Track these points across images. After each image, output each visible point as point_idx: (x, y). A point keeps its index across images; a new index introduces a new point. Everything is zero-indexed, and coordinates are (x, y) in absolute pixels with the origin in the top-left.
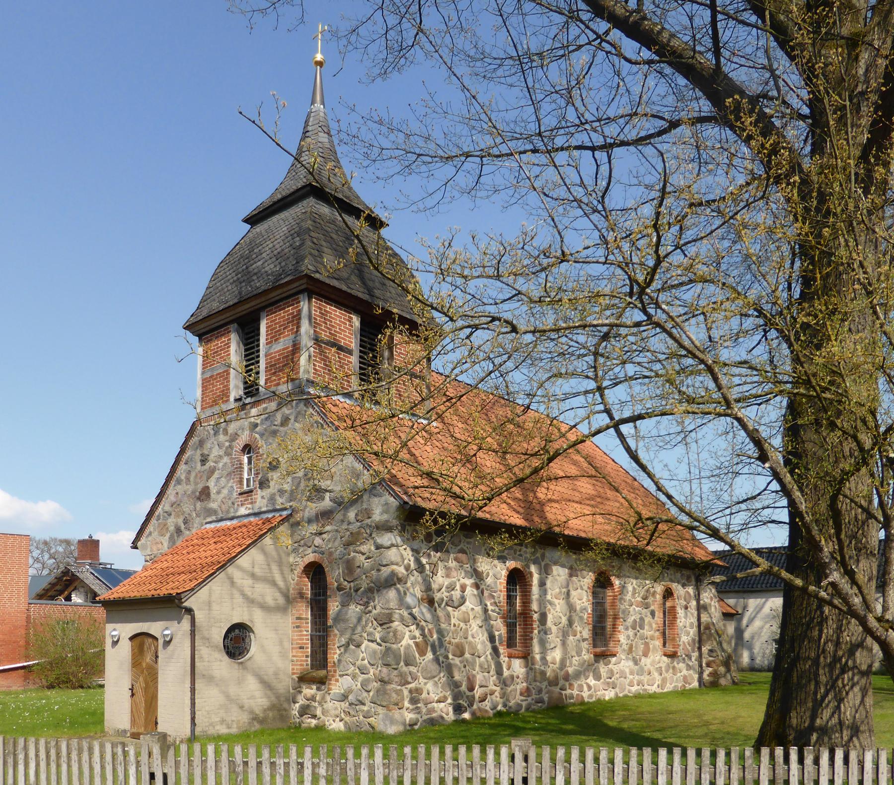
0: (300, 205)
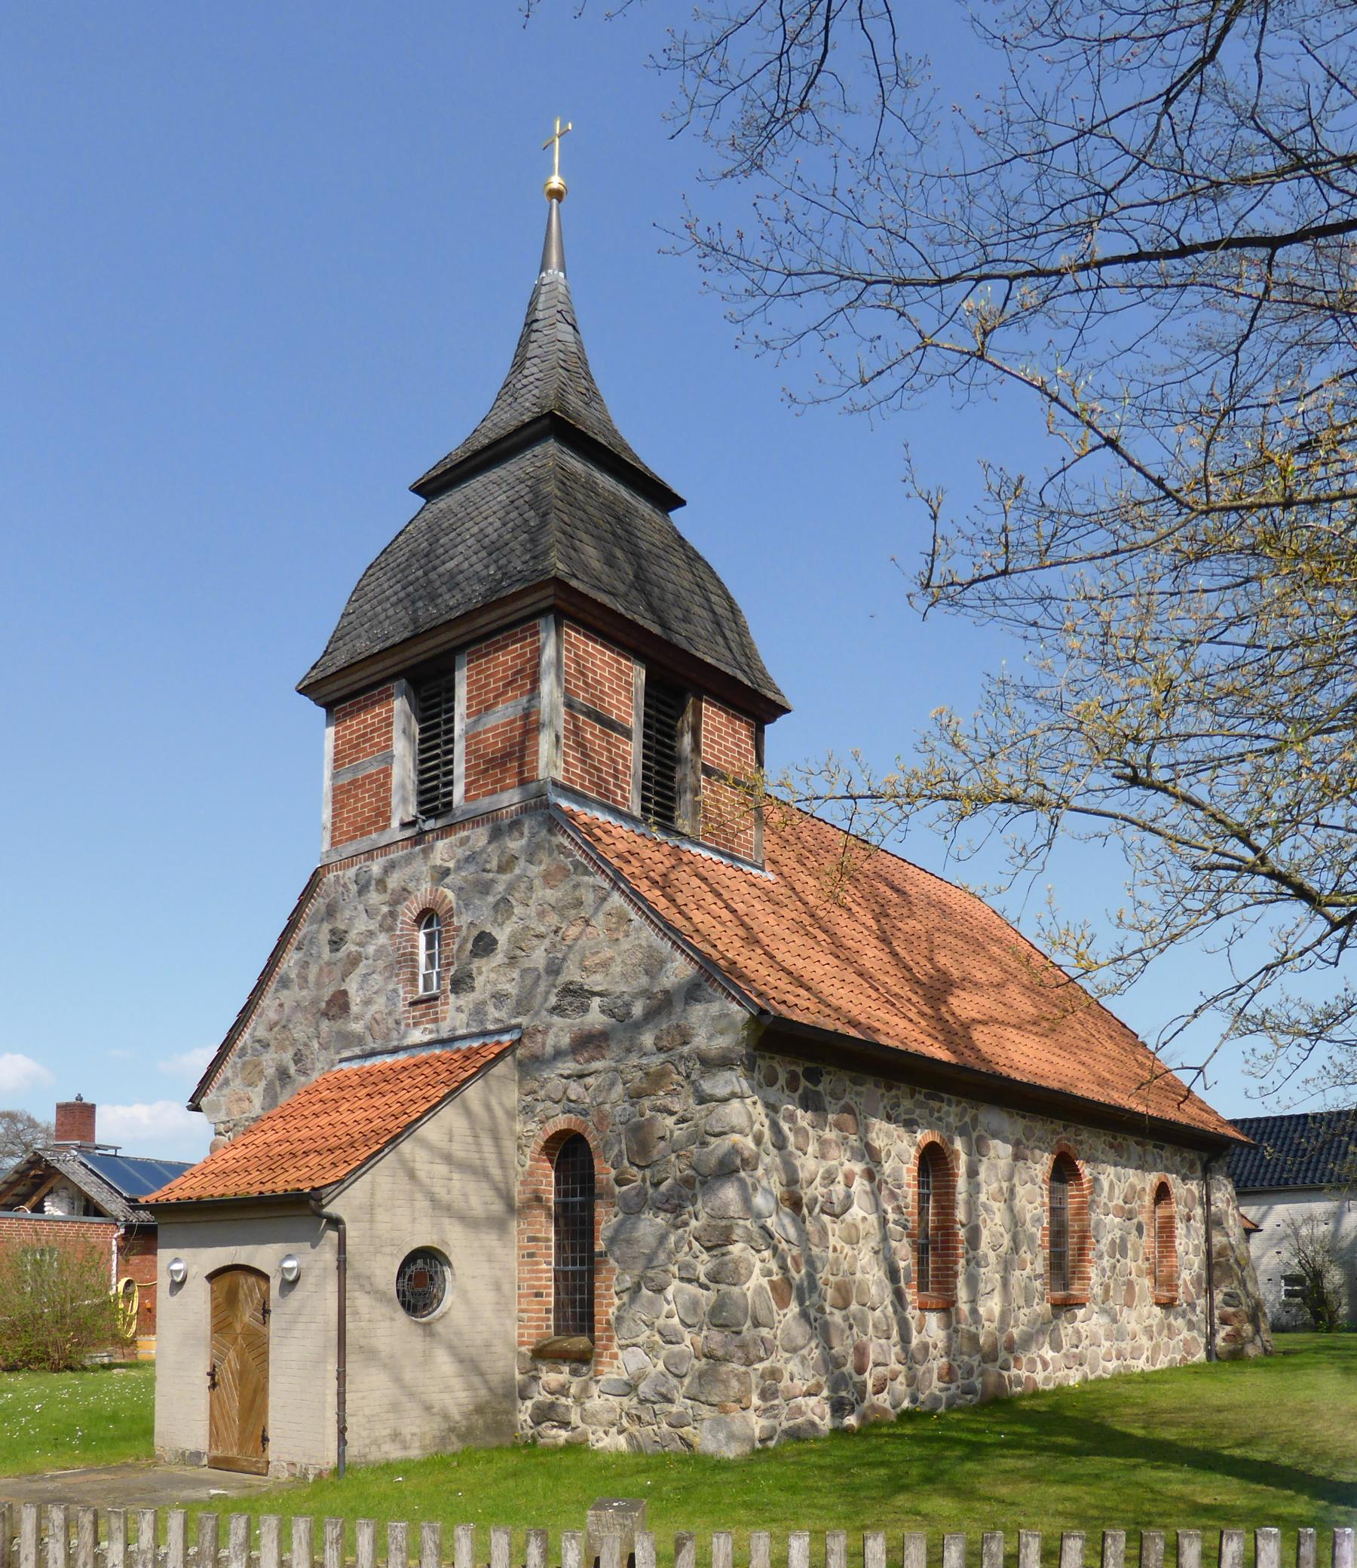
0: (529, 454)
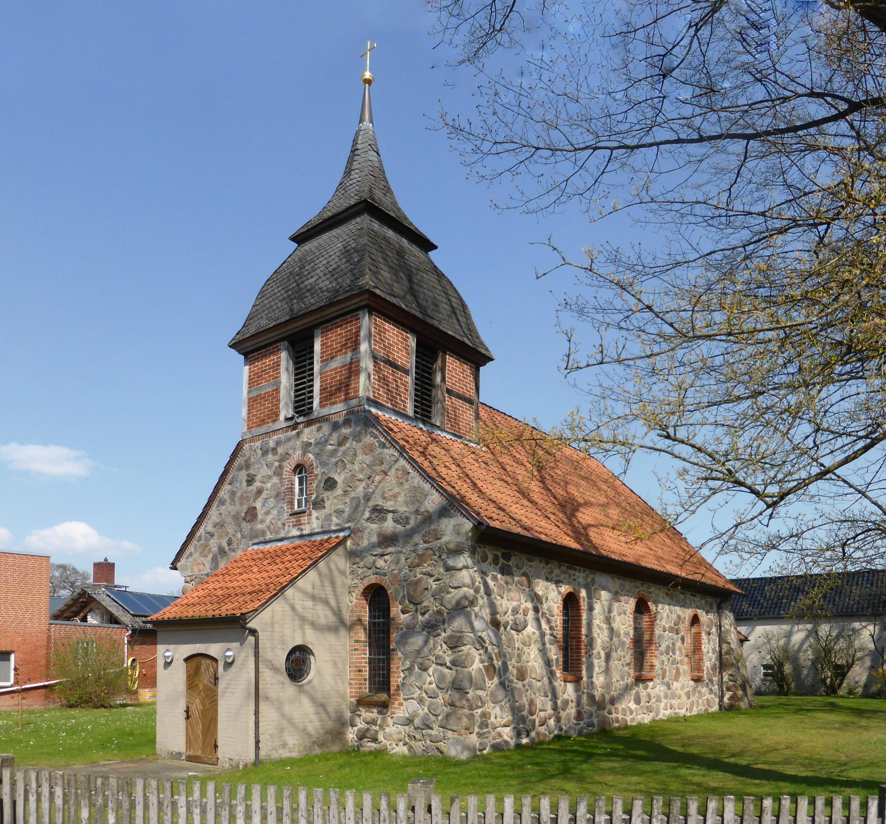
0: (353, 222)
